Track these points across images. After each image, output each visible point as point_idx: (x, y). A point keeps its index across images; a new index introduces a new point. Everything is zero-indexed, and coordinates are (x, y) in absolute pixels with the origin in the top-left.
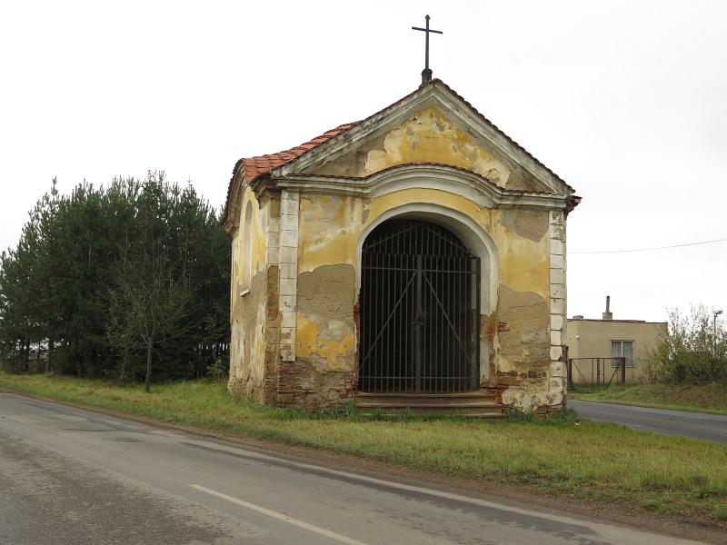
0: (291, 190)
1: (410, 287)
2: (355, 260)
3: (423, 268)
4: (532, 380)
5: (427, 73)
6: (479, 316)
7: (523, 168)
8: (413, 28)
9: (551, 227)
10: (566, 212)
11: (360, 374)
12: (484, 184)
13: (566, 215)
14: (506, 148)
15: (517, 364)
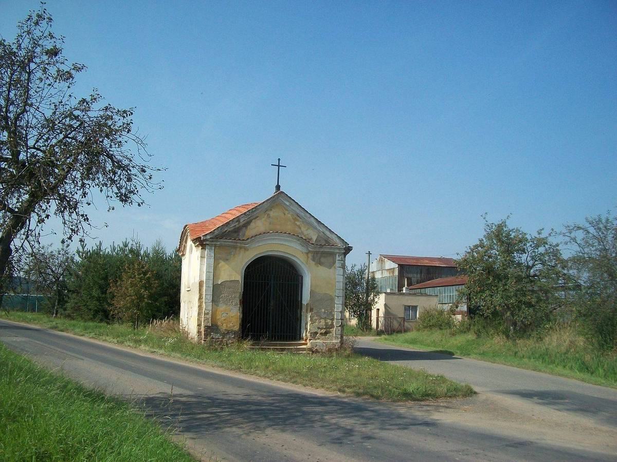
5: (278, 187)
6: (301, 304)
10: (345, 254)
12: (306, 242)
13: (345, 257)
14: (316, 224)
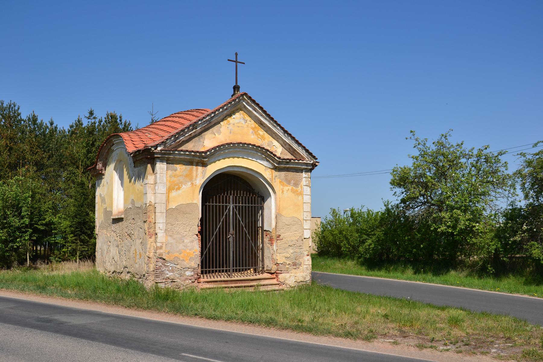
0: (162, 160)
1: (226, 215)
2: (198, 199)
3: (233, 203)
4: (295, 267)
7: (290, 145)
8: (229, 60)
9: (304, 179)
11: (202, 268)
15: (287, 258)
